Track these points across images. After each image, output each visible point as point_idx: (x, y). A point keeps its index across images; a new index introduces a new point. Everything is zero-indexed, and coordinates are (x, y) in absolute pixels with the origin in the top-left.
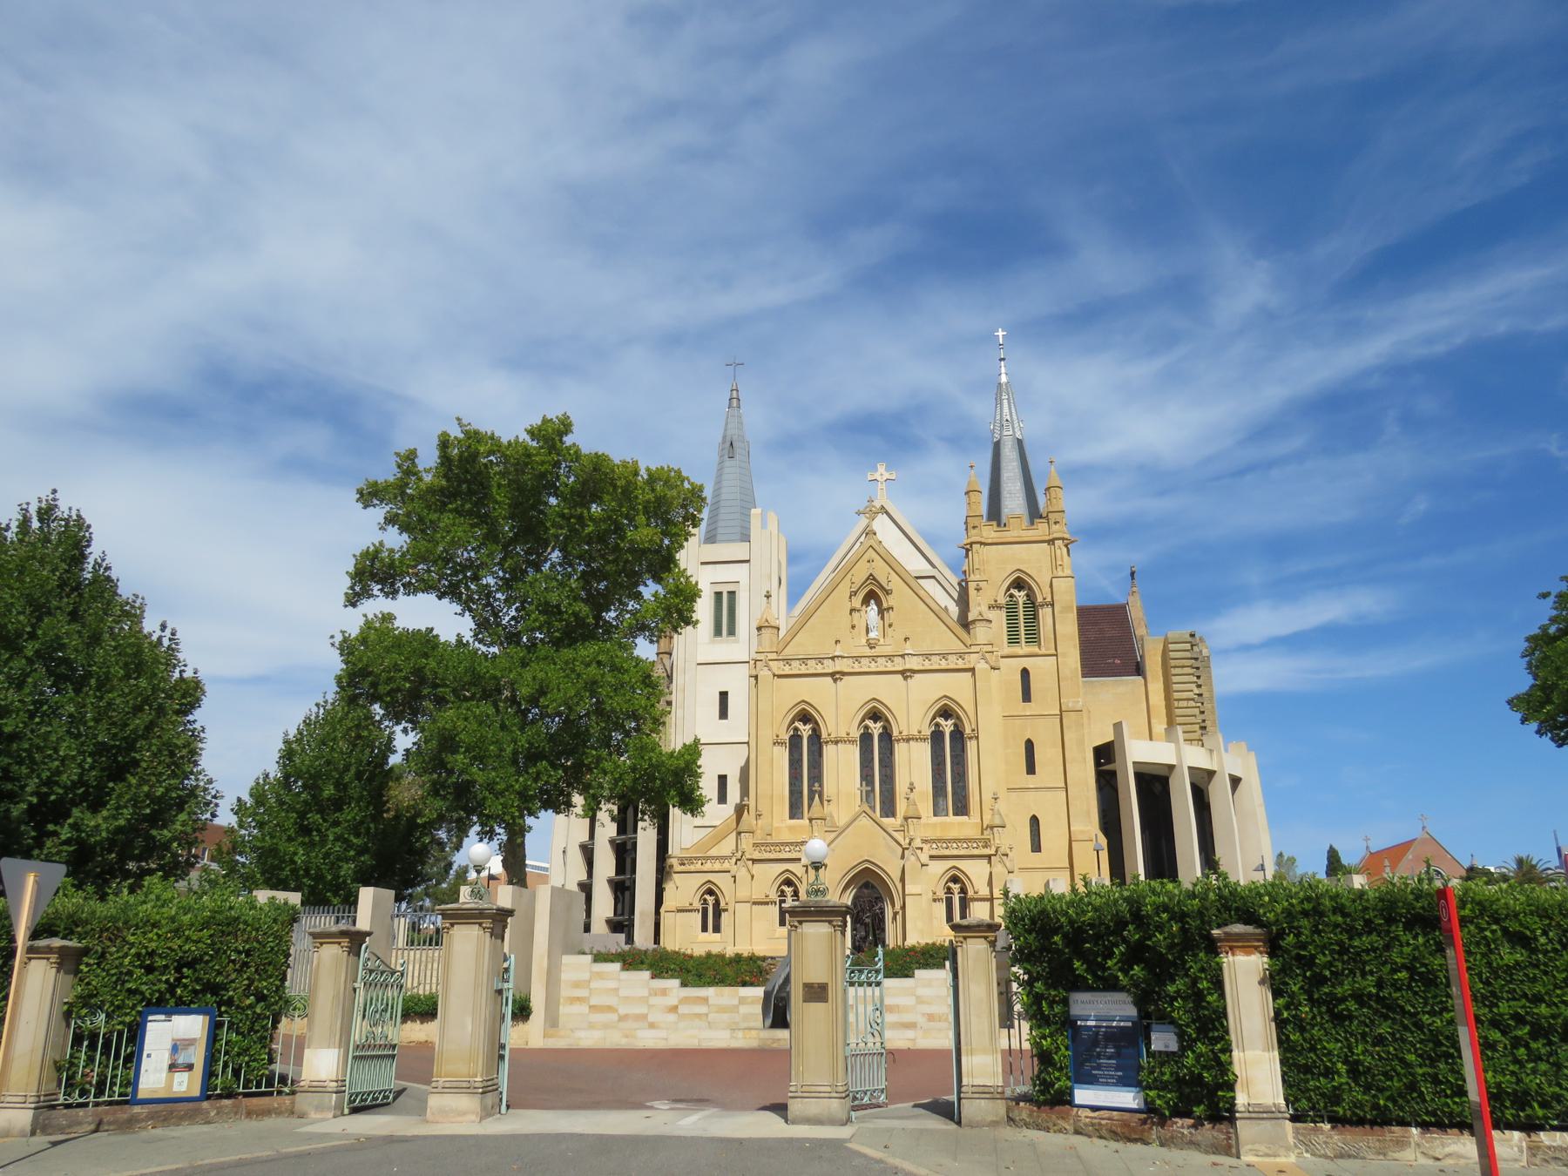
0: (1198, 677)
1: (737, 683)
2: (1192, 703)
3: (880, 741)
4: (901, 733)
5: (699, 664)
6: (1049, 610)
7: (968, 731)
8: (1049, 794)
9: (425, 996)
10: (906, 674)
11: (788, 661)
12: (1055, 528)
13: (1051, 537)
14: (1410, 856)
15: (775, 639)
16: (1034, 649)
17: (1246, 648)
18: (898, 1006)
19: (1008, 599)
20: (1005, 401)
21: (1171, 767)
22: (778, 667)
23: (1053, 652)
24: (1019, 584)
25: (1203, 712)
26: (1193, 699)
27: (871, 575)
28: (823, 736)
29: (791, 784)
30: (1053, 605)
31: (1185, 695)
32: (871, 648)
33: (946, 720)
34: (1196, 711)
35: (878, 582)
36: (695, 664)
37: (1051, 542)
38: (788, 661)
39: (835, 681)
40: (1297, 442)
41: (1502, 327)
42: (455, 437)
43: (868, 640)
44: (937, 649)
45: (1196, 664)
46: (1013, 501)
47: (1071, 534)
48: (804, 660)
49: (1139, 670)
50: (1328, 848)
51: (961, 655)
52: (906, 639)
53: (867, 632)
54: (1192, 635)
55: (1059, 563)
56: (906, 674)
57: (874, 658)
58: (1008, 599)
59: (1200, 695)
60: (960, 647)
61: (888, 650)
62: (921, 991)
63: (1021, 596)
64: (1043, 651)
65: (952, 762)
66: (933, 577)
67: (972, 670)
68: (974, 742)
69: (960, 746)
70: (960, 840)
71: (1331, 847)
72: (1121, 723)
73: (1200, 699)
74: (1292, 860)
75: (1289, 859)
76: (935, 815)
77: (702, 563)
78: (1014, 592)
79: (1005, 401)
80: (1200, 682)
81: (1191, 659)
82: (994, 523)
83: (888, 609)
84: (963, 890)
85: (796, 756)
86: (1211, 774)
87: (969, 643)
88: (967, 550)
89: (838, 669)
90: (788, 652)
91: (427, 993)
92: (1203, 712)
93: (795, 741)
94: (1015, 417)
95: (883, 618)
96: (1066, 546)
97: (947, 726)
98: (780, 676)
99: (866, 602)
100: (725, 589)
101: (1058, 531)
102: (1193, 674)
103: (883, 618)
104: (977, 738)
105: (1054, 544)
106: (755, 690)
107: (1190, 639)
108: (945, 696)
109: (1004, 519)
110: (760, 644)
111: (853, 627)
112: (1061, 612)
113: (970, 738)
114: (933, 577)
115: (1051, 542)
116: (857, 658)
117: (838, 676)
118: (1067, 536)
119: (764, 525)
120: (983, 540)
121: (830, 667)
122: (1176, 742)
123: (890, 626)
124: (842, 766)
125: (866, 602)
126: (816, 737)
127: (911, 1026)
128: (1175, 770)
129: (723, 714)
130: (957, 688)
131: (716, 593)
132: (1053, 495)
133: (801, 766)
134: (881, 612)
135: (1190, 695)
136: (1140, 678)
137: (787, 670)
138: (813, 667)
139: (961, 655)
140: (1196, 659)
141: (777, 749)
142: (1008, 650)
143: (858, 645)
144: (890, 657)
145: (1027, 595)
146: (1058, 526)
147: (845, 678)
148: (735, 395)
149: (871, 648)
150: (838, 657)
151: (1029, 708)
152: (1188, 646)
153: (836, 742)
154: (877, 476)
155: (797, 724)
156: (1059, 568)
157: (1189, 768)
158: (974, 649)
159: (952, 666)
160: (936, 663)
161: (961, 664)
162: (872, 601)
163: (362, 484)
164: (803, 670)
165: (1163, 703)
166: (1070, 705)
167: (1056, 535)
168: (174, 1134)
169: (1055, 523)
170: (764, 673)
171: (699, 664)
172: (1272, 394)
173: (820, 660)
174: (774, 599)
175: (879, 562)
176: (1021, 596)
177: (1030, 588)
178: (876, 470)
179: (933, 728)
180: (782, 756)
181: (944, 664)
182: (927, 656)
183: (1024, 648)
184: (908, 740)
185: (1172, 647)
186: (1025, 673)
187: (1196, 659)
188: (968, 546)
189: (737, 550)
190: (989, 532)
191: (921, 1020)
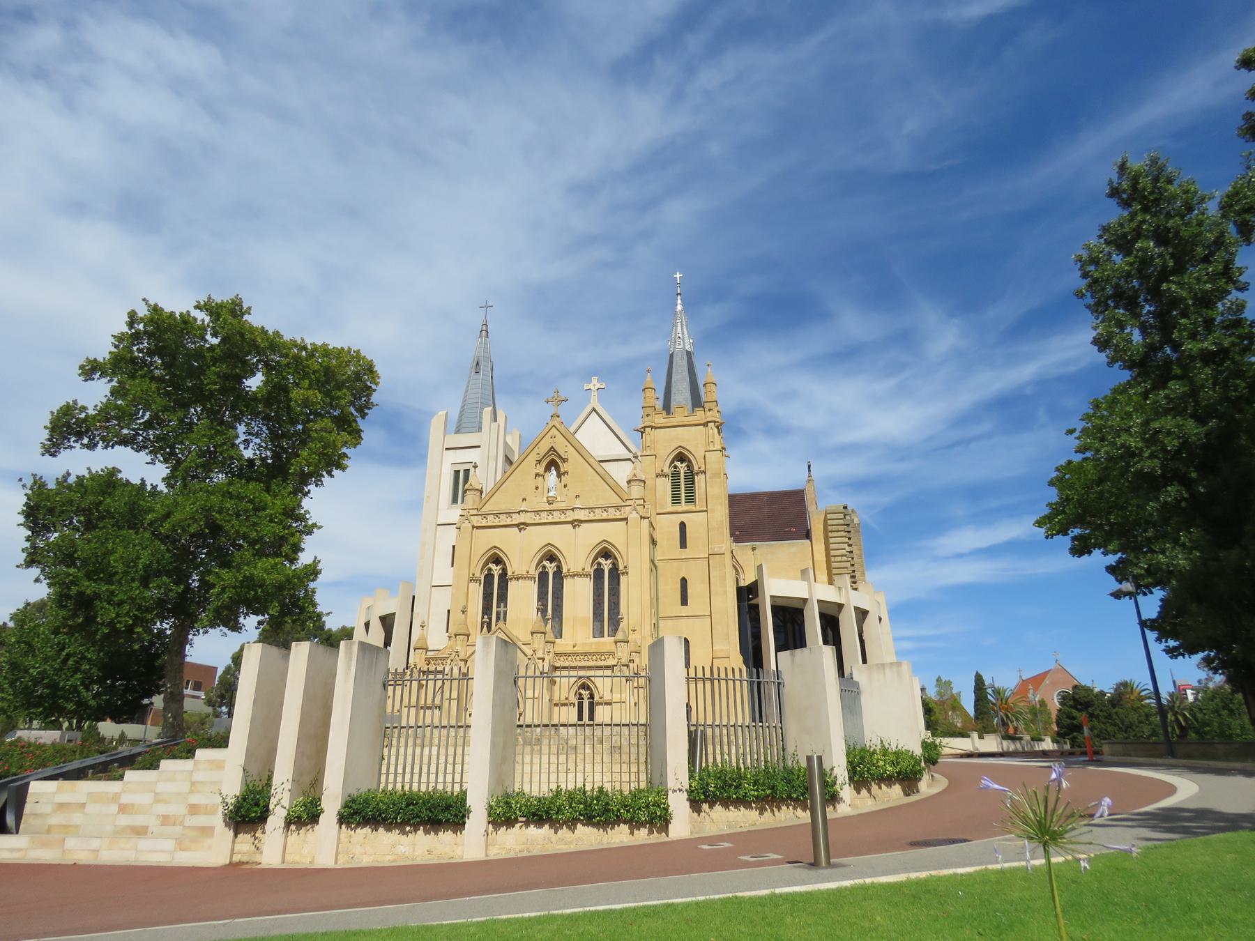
0: (850, 539)
2: (845, 559)
5: (438, 525)
7: (621, 567)
10: (575, 523)
11: (485, 515)
12: (709, 413)
13: (705, 421)
14: (1047, 682)
15: (477, 498)
16: (691, 507)
17: (960, 556)
18: (133, 805)
20: (679, 324)
21: (805, 601)
22: (477, 521)
24: (681, 457)
25: (853, 565)
26: (845, 555)
27: (552, 447)
30: (705, 473)
32: (549, 504)
33: (606, 560)
34: (848, 564)
35: (558, 454)
37: (705, 425)
38: (485, 515)
40: (986, 427)
46: (681, 394)
48: (497, 515)
49: (808, 535)
51: (618, 508)
52: (577, 496)
56: (575, 523)
57: (550, 512)
58: (673, 469)
59: (851, 552)
60: (618, 501)
61: (562, 505)
62: (161, 787)
63: (682, 467)
64: (698, 508)
65: (609, 594)
66: (629, 459)
67: (626, 519)
70: (590, 654)
71: (977, 672)
73: (851, 555)
74: (949, 683)
76: (594, 637)
77: (447, 449)
78: (678, 464)
79: (679, 324)
83: (564, 474)
86: (840, 606)
88: (642, 433)
90: (487, 509)
91: (390, 787)
92: (853, 565)
94: (686, 335)
96: (717, 427)
98: (478, 528)
99: (547, 469)
100: (462, 468)
101: (711, 416)
105: (707, 426)
107: (843, 510)
108: (605, 541)
111: (537, 488)
112: (710, 478)
113: (623, 574)
114: (629, 459)
115: (705, 425)
116: (537, 512)
118: (717, 420)
120: (654, 425)
121: (518, 519)
124: (523, 597)
125: (547, 469)
126: (504, 576)
127: (140, 831)
128: (808, 603)
130: (613, 534)
134: (559, 476)
135: (843, 552)
136: (808, 541)
137: (484, 523)
138: (504, 520)
139: (618, 508)
140: (848, 525)
142: (670, 508)
144: (563, 511)
145: (688, 466)
148: (484, 329)
149: (549, 504)
150: (522, 511)
151: (684, 554)
154: (591, 386)
157: (818, 601)
158: (628, 503)
159: (611, 517)
160: (599, 514)
161: (618, 515)
162: (553, 468)
163: (82, 361)
164: (496, 522)
168: (563, 846)
169: (709, 410)
171: (438, 525)
172: (966, 398)
175: (560, 438)
176: (682, 467)
177: (690, 461)
178: (590, 382)
179: (596, 567)
180: (477, 591)
182: (592, 509)
183: (684, 506)
184: (573, 576)
185: (829, 516)
186: (683, 525)
187: (848, 525)
188: (642, 430)
190: (660, 420)
191: (152, 822)
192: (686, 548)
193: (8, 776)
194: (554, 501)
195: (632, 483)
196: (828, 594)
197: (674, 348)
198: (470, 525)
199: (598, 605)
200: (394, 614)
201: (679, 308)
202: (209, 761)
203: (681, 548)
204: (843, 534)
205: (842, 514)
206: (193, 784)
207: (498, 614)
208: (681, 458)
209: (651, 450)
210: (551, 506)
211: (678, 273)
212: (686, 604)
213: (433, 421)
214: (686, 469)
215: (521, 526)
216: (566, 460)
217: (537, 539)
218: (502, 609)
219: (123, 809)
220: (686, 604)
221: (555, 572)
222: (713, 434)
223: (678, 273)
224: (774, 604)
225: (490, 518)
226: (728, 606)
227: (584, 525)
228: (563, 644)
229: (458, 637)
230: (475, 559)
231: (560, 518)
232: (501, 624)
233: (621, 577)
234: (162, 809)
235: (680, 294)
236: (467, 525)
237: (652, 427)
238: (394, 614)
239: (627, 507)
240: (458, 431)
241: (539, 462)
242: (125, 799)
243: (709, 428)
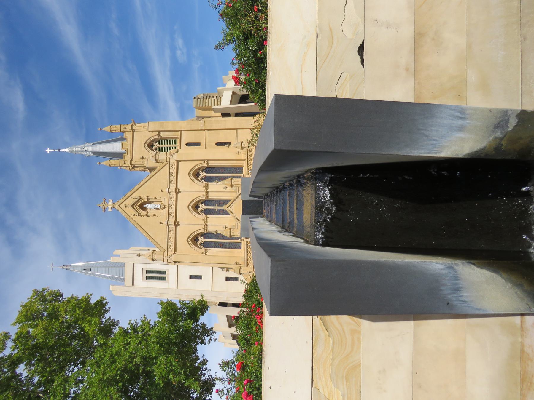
0: (210, 97)
1: (186, 271)
3: (208, 205)
4: (204, 195)
5: (177, 288)
6: (162, 133)
7: (204, 165)
10: (177, 192)
11: (168, 247)
12: (127, 129)
13: (131, 131)
16: (178, 141)
21: (234, 93)
22: (171, 251)
23: (180, 132)
26: (218, 99)
27: (132, 206)
28: (204, 231)
29: (226, 248)
30: (160, 131)
36: (177, 290)
39: (179, 225)
41: (168, 73)
42: (239, 313)
43: (161, 209)
44: (167, 177)
45: (205, 97)
48: (169, 239)
51: (171, 166)
52: (162, 191)
53: (157, 209)
54: (195, 98)
55: (142, 128)
56: (177, 192)
57: (170, 206)
59: (216, 97)
60: (167, 167)
61: (166, 199)
64: (179, 137)
65: (219, 173)
67: (178, 161)
68: (210, 162)
73: (218, 97)
77: (133, 285)
81: (203, 99)
82: (124, 155)
83: (148, 199)
85: (213, 244)
87: (166, 163)
89: (173, 223)
90: (164, 246)
93: (206, 245)
95: (153, 202)
97: (203, 174)
99: (144, 209)
100: (145, 275)
102: (209, 99)
103: (153, 202)
104: (208, 160)
105: (134, 130)
106: (181, 263)
107: (196, 99)
109: (124, 151)
110: (160, 260)
111: (155, 215)
113: (208, 164)
115: (133, 131)
116: (169, 214)
117: (176, 223)
119: (118, 256)
121: (172, 227)
123: (155, 198)
125: (144, 209)
129: (199, 277)
130: (185, 168)
131: (146, 279)
133: (218, 242)
134: (150, 202)
135: (216, 100)
137: (173, 247)
138: (172, 235)
139: (171, 166)
140: (203, 97)
141: (208, 253)
143: (163, 214)
144: (170, 199)
145: (156, 142)
146: (127, 128)
147: (178, 220)
150: (167, 223)
152: (199, 100)
153: (207, 225)
155: (198, 244)
156: (145, 128)
158: (168, 160)
159: (175, 170)
160: (173, 178)
161: (175, 167)
162: (144, 206)
166: (202, 126)
170: (173, 258)
174: (141, 252)
180: (212, 251)
182: (170, 182)
183: (178, 144)
184: (207, 192)
185: (198, 106)
186: (188, 144)
187: (203, 97)
188: (132, 166)
189: (128, 269)
193: (289, 207)
194: (163, 205)
197: (90, 152)
200: (227, 316)
201: (67, 150)
203: (200, 146)
204: (207, 100)
205: (198, 99)
208: (151, 146)
209: (145, 161)
210: (166, 206)
213: (115, 295)
214: (157, 143)
215: (176, 224)
216: (140, 198)
221: (205, 205)
222: (139, 126)
223: (46, 150)
224: (234, 116)
225: (170, 243)
226: (231, 122)
227: (179, 187)
229: (241, 272)
235: (59, 150)
237: (132, 160)
238: (227, 316)
239: (171, 161)
240: (123, 280)
243: (135, 128)
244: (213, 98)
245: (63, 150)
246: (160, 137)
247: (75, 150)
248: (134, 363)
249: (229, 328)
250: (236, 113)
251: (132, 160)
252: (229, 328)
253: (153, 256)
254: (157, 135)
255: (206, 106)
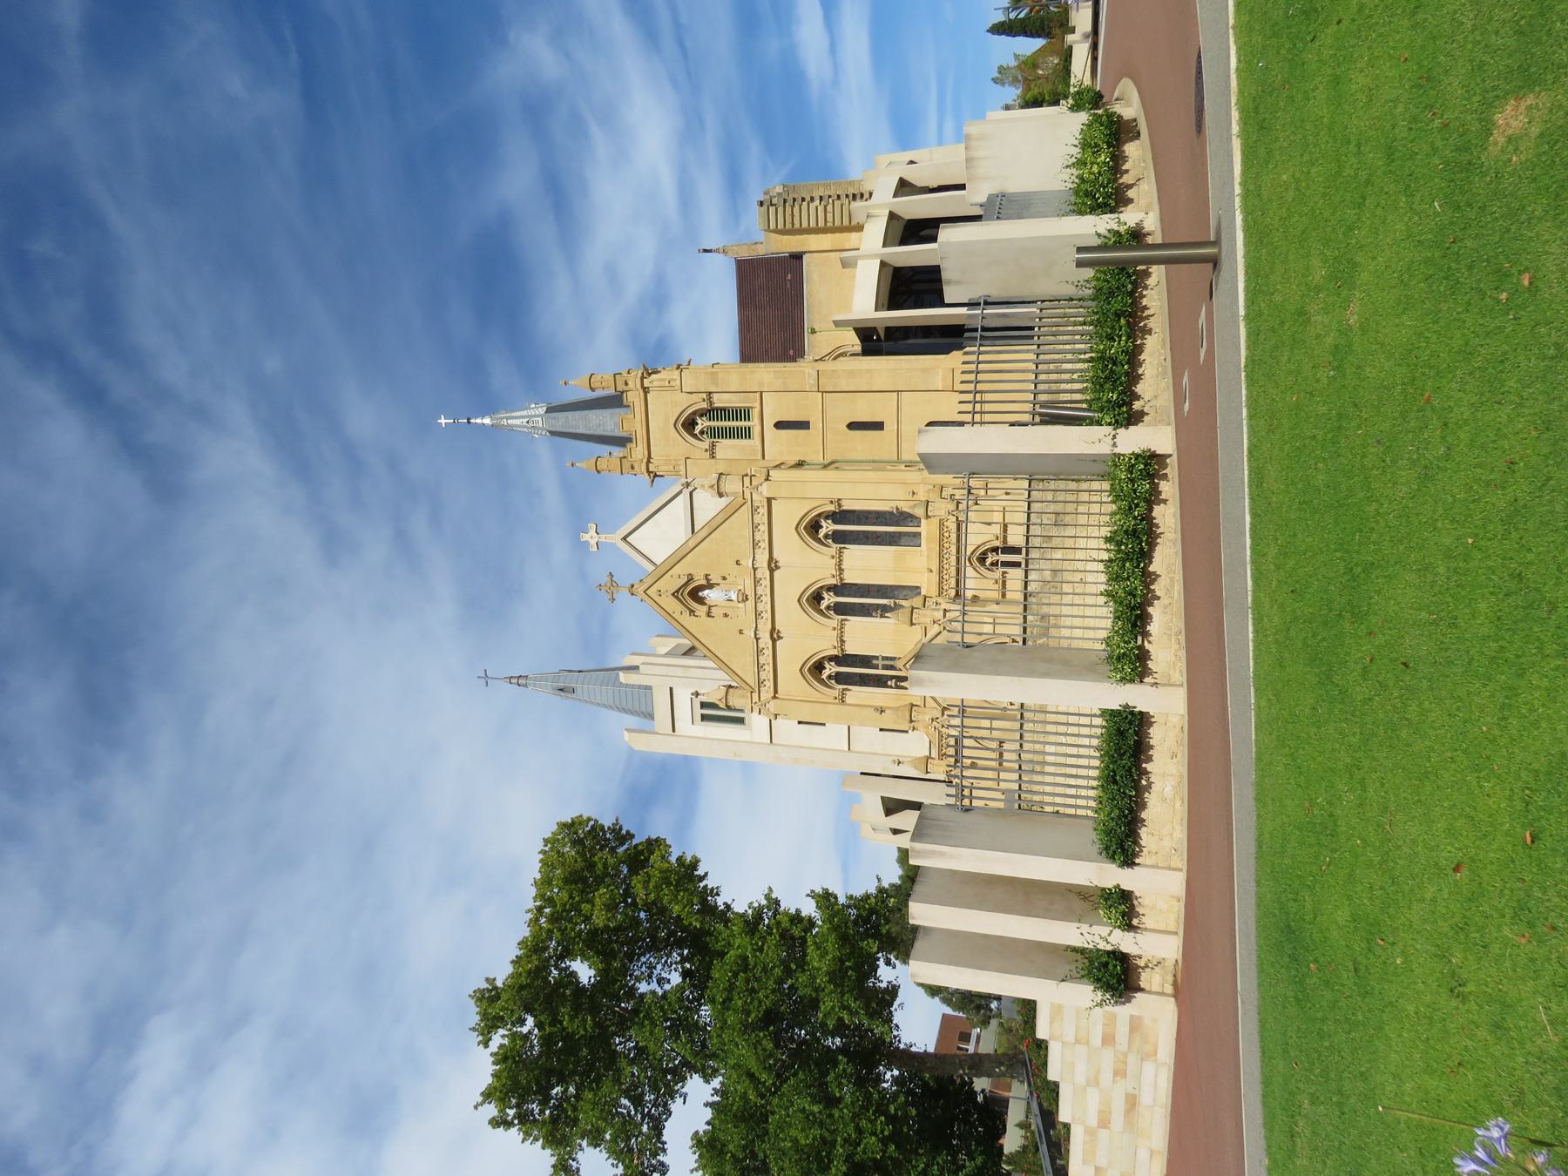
0: (803, 200)
2: (829, 208)
3: (843, 595)
7: (832, 508)
8: (905, 409)
9: (1113, 502)
10: (773, 566)
11: (760, 683)
13: (641, 391)
16: (755, 413)
17: (833, 48)
18: (1100, 1112)
19: (705, 436)
21: (883, 264)
22: (767, 692)
24: (690, 425)
26: (825, 207)
27: (673, 594)
30: (710, 393)
31: (821, 214)
32: (747, 599)
35: (681, 588)
36: (771, 747)
37: (646, 390)
38: (760, 683)
47: (639, 369)
48: (760, 667)
49: (797, 257)
50: (990, 34)
51: (754, 510)
52: (738, 563)
56: (773, 566)
57: (757, 598)
58: (705, 436)
61: (749, 583)
62: (1080, 1079)
64: (757, 404)
65: (865, 524)
67: (769, 500)
69: (849, 515)
71: (988, 31)
72: (834, 321)
73: (826, 199)
74: (1001, 70)
75: (1000, 72)
76: (920, 546)
77: (674, 731)
80: (808, 199)
83: (708, 580)
84: (995, 550)
86: (892, 216)
88: (656, 476)
90: (752, 680)
91: (1092, 804)
92: (839, 197)
96: (650, 374)
98: (776, 691)
99: (701, 601)
100: (699, 712)
101: (634, 383)
102: (800, 206)
105: (648, 388)
107: (765, 207)
108: (796, 528)
111: (726, 615)
112: (717, 385)
113: (840, 505)
115: (646, 390)
116: (758, 615)
117: (775, 636)
118: (640, 375)
120: (645, 460)
122: (856, 259)
124: (865, 636)
125: (701, 601)
127: (1132, 1102)
130: (788, 517)
131: (702, 720)
132: (598, 385)
133: (868, 675)
134: (710, 586)
135: (821, 209)
136: (804, 257)
138: (766, 658)
139: (754, 510)
140: (785, 201)
144: (756, 582)
145: (701, 416)
146: (629, 383)
149: (747, 599)
150: (756, 634)
151: (816, 424)
152: (772, 209)
154: (593, 542)
156: (672, 383)
158: (748, 496)
159: (765, 519)
160: (762, 535)
161: (764, 511)
162: (700, 594)
165: (829, 236)
166: (812, 382)
167: (639, 386)
173: (759, 652)
176: (702, 423)
177: (694, 413)
180: (857, 694)
181: (764, 528)
182: (755, 545)
183: (754, 423)
184: (841, 570)
185: (772, 226)
186: (780, 425)
187: (785, 201)
188: (652, 475)
190: (638, 452)
192: (809, 422)
194: (743, 594)
195: (722, 490)
196: (875, 231)
198: (772, 702)
199: (879, 540)
200: (882, 797)
201: (487, 421)
202: (1051, 1023)
206: (1077, 1041)
207: (886, 667)
210: (749, 597)
211: (439, 421)
212: (882, 423)
214: (704, 418)
215: (775, 636)
216: (690, 577)
217: (791, 616)
218: (880, 662)
219: (1104, 1123)
220: (882, 423)
223: (439, 421)
228: (928, 585)
230: (816, 696)
231: (764, 532)
232: (899, 664)
233: (846, 581)
234: (1107, 1076)
235: (468, 419)
236: (773, 706)
237: (649, 462)
241: (692, 612)
242: (1093, 1121)
244: (811, 205)
245: (479, 421)
246: (711, 404)
247: (505, 423)
248: (674, 883)
249: (886, 816)
250: (886, 328)
251: (649, 462)
252: (886, 816)
253: (728, 700)
254: (704, 400)
255: (793, 226)
